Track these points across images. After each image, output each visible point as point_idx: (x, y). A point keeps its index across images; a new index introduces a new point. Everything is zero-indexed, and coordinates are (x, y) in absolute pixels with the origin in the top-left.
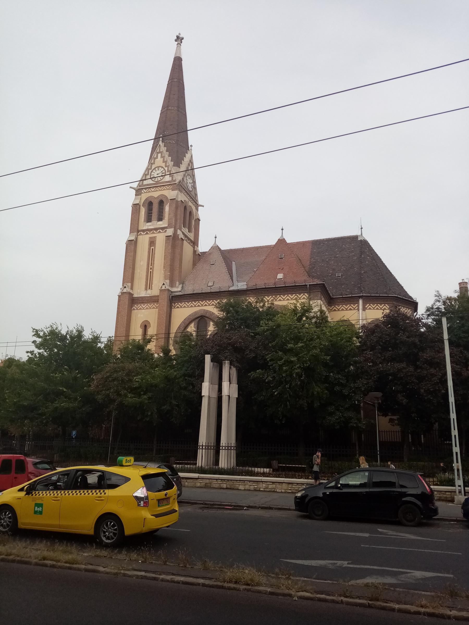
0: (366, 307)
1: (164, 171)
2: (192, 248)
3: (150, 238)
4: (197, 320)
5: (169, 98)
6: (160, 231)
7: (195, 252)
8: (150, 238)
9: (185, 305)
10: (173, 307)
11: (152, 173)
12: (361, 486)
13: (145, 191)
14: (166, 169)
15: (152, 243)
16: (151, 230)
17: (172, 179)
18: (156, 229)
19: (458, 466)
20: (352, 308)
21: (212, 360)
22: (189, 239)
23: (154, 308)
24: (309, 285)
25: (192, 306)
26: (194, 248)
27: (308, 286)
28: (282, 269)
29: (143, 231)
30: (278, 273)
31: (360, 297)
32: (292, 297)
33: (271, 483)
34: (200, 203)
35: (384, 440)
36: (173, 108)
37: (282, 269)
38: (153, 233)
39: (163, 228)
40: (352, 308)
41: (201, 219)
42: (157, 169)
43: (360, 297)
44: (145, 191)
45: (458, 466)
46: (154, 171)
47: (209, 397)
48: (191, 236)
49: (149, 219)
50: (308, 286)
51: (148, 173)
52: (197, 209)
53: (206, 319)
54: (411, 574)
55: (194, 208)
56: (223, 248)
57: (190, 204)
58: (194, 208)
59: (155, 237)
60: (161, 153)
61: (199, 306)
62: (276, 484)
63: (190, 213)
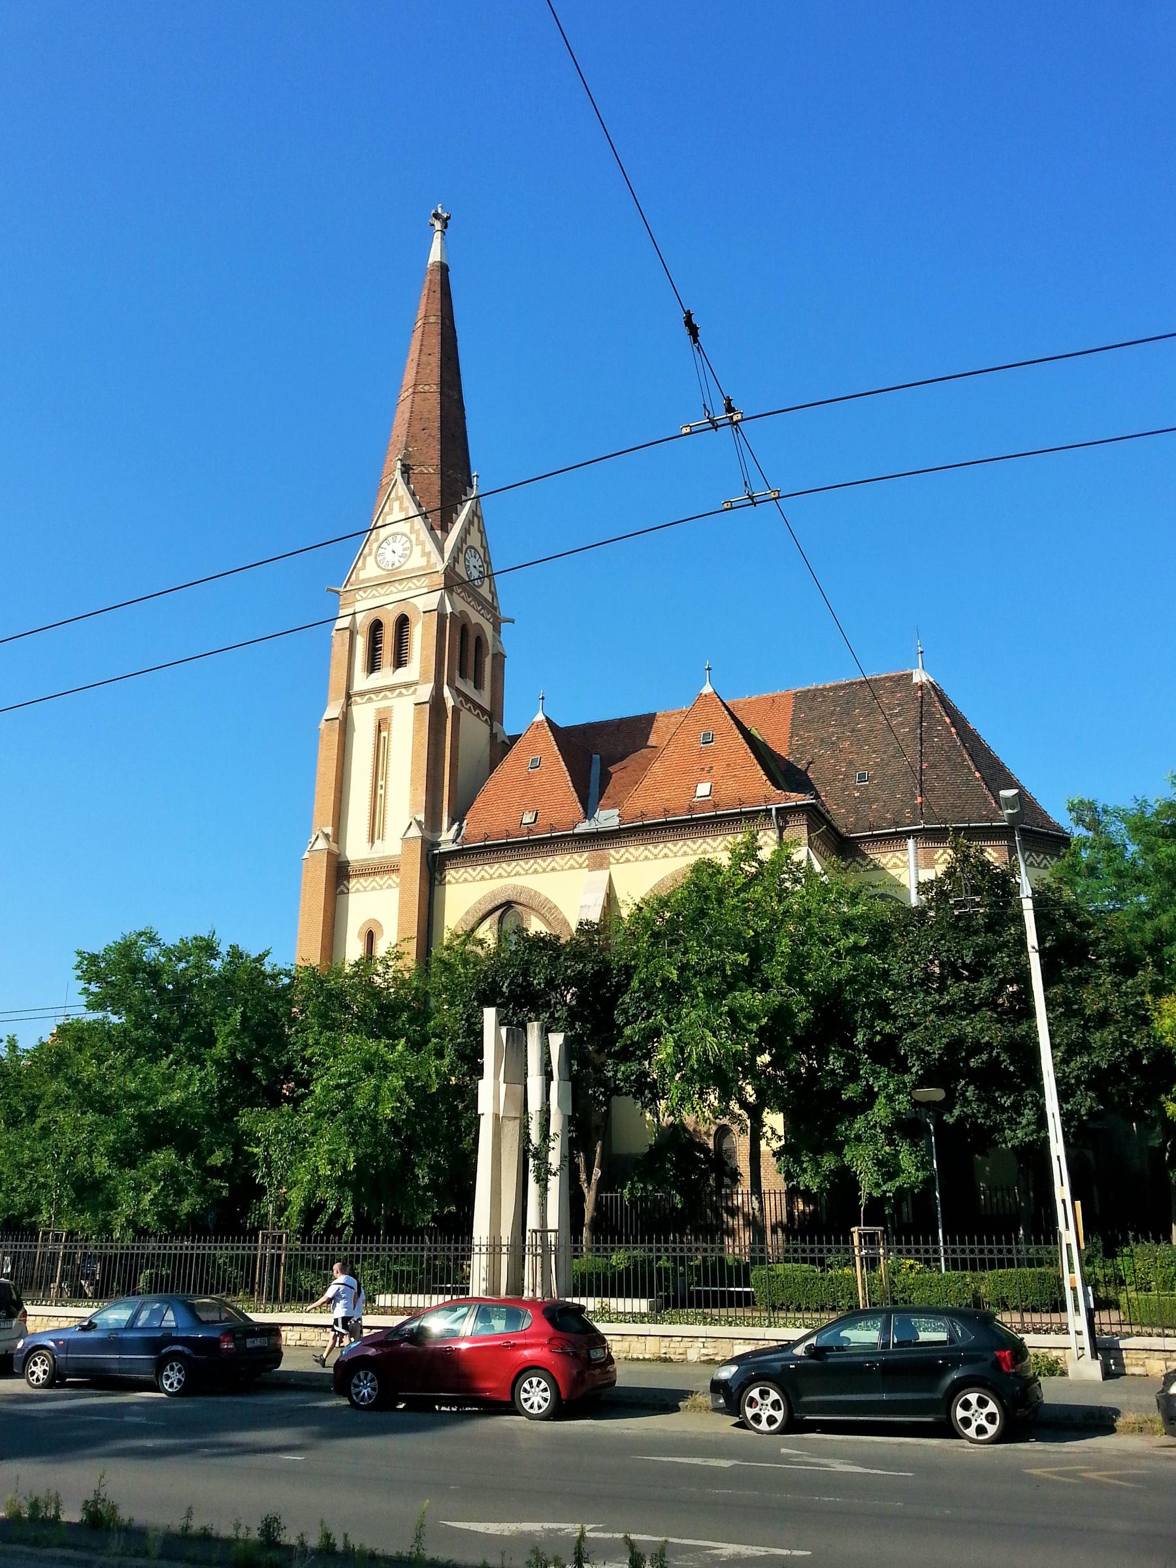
0: (936, 857)
1: (408, 545)
2: (487, 728)
3: (379, 711)
4: (499, 913)
5: (418, 365)
6: (370, 699)
7: (493, 736)
8: (379, 711)
9: (466, 875)
10: (437, 883)
11: (381, 551)
12: (1129, 1335)
13: (364, 595)
14: (413, 537)
15: (381, 725)
16: (377, 691)
17: (428, 561)
18: (392, 688)
19: (1072, 1281)
20: (899, 862)
21: (501, 1022)
22: (477, 706)
23: (390, 887)
24: (777, 809)
25: (483, 878)
26: (491, 726)
27: (774, 812)
28: (709, 772)
29: (362, 694)
30: (700, 781)
31: (908, 834)
32: (636, 854)
33: (619, 1338)
34: (504, 612)
35: (995, 1212)
36: (427, 388)
37: (709, 772)
38: (386, 698)
39: (407, 685)
40: (899, 862)
41: (507, 652)
42: (390, 539)
43: (908, 834)
44: (364, 595)
45: (1072, 1281)
46: (384, 545)
47: (496, 1116)
48: (484, 699)
49: (373, 666)
50: (774, 812)
51: (371, 550)
52: (497, 629)
53: (520, 907)
54: (715, 1552)
55: (488, 629)
56: (562, 724)
57: (475, 617)
58: (488, 629)
59: (389, 709)
60: (398, 498)
61: (500, 876)
62: (630, 1338)
63: (480, 642)
